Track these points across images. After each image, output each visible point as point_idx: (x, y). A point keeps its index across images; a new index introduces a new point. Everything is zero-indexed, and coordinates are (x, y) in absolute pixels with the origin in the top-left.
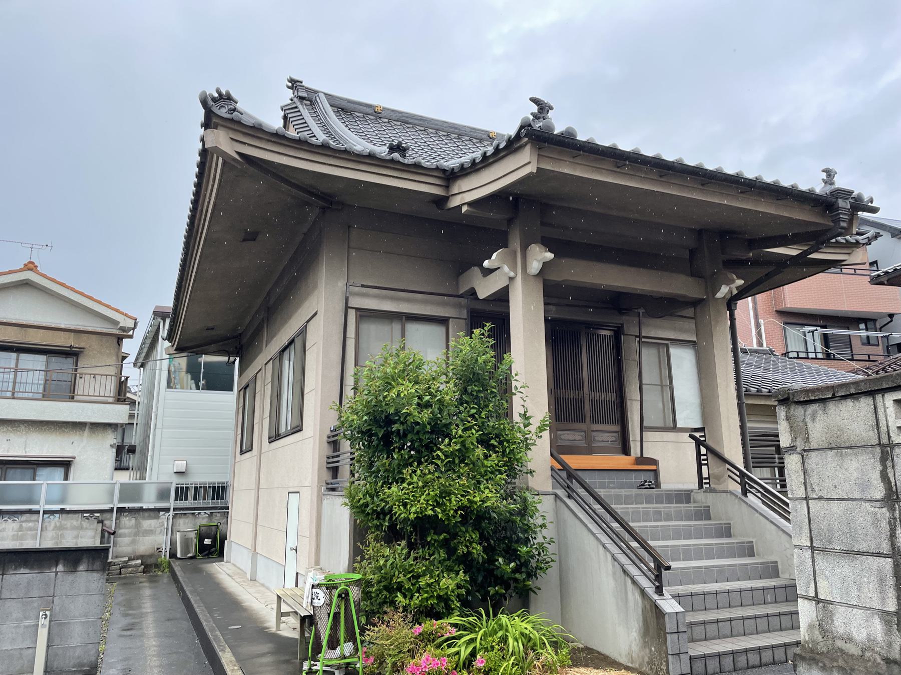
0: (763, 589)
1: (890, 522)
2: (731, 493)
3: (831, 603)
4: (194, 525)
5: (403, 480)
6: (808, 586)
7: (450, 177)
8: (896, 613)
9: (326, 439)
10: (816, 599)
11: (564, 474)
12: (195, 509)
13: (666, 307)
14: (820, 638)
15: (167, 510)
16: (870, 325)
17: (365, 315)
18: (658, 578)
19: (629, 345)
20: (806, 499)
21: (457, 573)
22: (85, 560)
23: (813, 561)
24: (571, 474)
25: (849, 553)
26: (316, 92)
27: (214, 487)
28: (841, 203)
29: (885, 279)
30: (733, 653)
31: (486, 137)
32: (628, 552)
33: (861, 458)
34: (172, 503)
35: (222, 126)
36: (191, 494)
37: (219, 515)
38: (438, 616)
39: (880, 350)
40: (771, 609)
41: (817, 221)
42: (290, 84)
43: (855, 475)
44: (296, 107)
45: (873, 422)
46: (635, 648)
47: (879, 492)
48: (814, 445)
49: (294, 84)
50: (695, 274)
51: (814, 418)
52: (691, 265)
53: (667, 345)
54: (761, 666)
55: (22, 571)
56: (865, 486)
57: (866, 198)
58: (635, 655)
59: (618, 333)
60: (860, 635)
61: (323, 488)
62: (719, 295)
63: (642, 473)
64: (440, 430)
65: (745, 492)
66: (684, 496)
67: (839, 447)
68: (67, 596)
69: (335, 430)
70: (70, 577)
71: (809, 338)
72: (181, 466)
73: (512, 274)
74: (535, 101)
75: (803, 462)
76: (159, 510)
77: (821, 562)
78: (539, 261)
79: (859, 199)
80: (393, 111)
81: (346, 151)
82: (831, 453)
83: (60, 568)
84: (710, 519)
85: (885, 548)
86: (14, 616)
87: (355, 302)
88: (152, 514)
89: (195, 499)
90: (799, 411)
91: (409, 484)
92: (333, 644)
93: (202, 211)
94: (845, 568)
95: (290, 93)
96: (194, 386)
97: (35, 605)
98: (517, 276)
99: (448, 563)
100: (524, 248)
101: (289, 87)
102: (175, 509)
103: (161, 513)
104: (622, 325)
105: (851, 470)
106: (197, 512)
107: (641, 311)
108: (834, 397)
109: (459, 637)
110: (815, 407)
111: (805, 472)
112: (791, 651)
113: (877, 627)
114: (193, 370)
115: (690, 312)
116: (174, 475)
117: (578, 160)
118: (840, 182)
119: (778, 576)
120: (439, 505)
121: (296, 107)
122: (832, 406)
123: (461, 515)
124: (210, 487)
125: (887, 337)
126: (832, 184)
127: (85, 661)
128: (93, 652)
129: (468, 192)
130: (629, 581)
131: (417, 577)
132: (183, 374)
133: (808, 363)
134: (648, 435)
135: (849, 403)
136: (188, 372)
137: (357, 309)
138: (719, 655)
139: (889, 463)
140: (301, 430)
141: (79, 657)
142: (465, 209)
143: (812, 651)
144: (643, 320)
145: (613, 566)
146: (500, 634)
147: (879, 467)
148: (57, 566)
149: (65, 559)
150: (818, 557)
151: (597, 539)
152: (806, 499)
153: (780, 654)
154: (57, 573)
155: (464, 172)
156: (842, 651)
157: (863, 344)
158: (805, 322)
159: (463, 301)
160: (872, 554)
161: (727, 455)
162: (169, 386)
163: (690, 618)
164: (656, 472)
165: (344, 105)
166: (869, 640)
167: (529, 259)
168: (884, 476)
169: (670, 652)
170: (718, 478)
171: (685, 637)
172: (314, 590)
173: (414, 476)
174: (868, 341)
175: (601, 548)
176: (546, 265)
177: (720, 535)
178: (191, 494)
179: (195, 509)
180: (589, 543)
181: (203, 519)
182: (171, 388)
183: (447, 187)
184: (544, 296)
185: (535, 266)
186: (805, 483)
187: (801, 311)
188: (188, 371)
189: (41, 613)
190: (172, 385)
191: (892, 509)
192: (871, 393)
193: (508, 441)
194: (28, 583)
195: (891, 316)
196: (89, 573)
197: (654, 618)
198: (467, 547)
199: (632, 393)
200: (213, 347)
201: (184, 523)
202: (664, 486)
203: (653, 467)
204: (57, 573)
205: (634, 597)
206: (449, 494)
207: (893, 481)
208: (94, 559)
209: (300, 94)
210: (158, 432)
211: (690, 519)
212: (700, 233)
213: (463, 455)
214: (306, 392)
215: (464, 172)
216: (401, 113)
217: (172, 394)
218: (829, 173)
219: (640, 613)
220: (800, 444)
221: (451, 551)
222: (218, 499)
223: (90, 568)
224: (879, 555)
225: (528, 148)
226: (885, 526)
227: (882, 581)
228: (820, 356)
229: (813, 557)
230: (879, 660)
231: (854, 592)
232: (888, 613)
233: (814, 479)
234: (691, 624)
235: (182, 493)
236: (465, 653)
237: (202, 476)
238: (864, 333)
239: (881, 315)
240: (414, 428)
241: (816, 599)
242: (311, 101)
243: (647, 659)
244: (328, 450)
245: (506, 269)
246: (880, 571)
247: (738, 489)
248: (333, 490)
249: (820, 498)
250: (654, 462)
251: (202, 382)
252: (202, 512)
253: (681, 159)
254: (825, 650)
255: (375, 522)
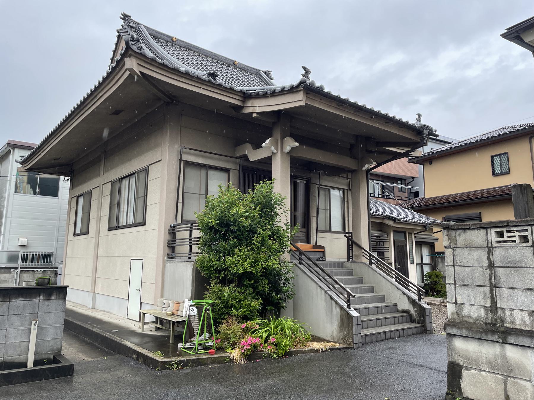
0: (382, 307)
1: (490, 275)
2: (364, 263)
3: (462, 304)
4: (34, 278)
5: (234, 254)
6: (452, 298)
7: (246, 96)
8: (490, 306)
9: (167, 231)
10: (456, 303)
11: (298, 253)
12: (34, 268)
13: (334, 171)
14: (457, 317)
15: (17, 268)
16: (403, 181)
17: (188, 164)
18: (349, 301)
19: (314, 189)
20: (454, 266)
21: (258, 299)
22: (55, 294)
23: (455, 289)
24: (301, 253)
25: (472, 286)
26: (139, 24)
27: (45, 255)
28: (425, 131)
29: (415, 161)
30: (376, 334)
31: (232, 63)
32: (334, 289)
33: (479, 251)
34: (20, 264)
35: (134, 56)
36: (30, 259)
37: (49, 272)
38: (251, 319)
39: (406, 195)
40: (384, 316)
41: (412, 138)
42: (122, 17)
43: (476, 257)
44: (127, 32)
45: (485, 238)
46: (336, 333)
47: (486, 263)
48: (459, 245)
49: (125, 17)
50: (353, 157)
51: (459, 235)
52: (350, 151)
53: (329, 190)
54: (385, 340)
55: (20, 299)
56: (480, 261)
57: (434, 129)
58: (335, 336)
59: (308, 182)
60: (474, 315)
61: (166, 257)
62: (364, 169)
63: (318, 253)
64: (252, 232)
65: (371, 263)
66: (340, 265)
67: (470, 247)
68: (45, 313)
69: (174, 227)
70: (47, 303)
71: (376, 186)
72: (23, 241)
73: (275, 151)
74: (304, 68)
75: (453, 252)
76: (11, 268)
77: (458, 289)
78: (290, 146)
79: (431, 130)
80: (183, 42)
81: (163, 65)
82: (466, 249)
83: (41, 298)
84: (352, 275)
85: (487, 283)
86: (16, 324)
87: (186, 157)
88: (6, 270)
89: (32, 262)
90: (453, 233)
91: (238, 256)
92: (202, 333)
93: (96, 96)
94: (470, 292)
95: (122, 22)
96: (32, 192)
97: (28, 318)
98: (277, 153)
99: (253, 295)
100: (283, 138)
101: (121, 18)
102: (21, 268)
103: (12, 270)
104: (311, 178)
105: (475, 255)
106: (36, 270)
107: (321, 172)
108: (470, 228)
109: (260, 329)
110: (461, 231)
111: (454, 255)
112: (397, 333)
113: (482, 312)
114: (32, 182)
115: (349, 175)
116: (19, 247)
117: (323, 101)
118: (423, 122)
119: (385, 302)
120: (252, 267)
121: (127, 32)
122: (468, 232)
123: (263, 272)
124: (36, 255)
125: (410, 188)
126: (420, 121)
127: (55, 348)
128: (59, 343)
129: (257, 107)
130: (334, 303)
131: (240, 301)
132: (25, 184)
133: (375, 199)
134: (319, 234)
135: (476, 231)
136: (28, 183)
137: (184, 161)
138: (371, 335)
139: (491, 254)
140: (145, 225)
141: (51, 346)
142: (254, 115)
143: (453, 322)
144: (321, 176)
145: (325, 296)
146: (280, 327)
147: (487, 255)
148: (39, 296)
149: (44, 293)
150: (457, 287)
151: (317, 284)
152: (454, 266)
153: (392, 335)
154: (39, 300)
155: (258, 96)
156: (466, 321)
157: (399, 191)
158: (374, 178)
159: (238, 161)
160: (482, 286)
161: (363, 246)
162: (16, 192)
163: (363, 319)
164: (324, 253)
165: (155, 33)
166: (478, 316)
167: (284, 145)
168: (489, 258)
169: (354, 333)
170: (358, 256)
171: (360, 327)
172: (191, 308)
173: (241, 252)
174: (401, 190)
175: (319, 288)
176: (293, 148)
177: (359, 283)
178: (30, 259)
179: (34, 268)
180: (312, 286)
181: (39, 274)
182: (18, 192)
183: (243, 102)
184: (291, 163)
185: (288, 149)
186: (453, 260)
187: (385, 175)
188: (28, 183)
189: (33, 323)
190: (18, 191)
191: (491, 270)
192: (486, 228)
193: (282, 237)
194: (24, 306)
195: (413, 178)
196: (57, 301)
197: (346, 320)
198: (263, 287)
199: (313, 213)
200: (49, 170)
201: (27, 276)
202: (327, 260)
203: (323, 250)
204: (39, 300)
205: (336, 311)
206: (258, 261)
207: (492, 260)
208: (59, 293)
209: (131, 25)
210: (9, 220)
211: (344, 275)
212: (357, 137)
213: (263, 243)
214: (148, 204)
215: (258, 96)
216: (187, 43)
217: (18, 197)
218: (419, 116)
219: (339, 316)
220: (452, 245)
221: (254, 289)
222: (47, 262)
223: (58, 298)
224: (484, 286)
225: (302, 93)
226: (487, 276)
227: (485, 296)
228: (380, 196)
229: (455, 288)
230: (482, 323)
231: (473, 300)
232: (487, 307)
233: (457, 259)
234: (362, 321)
235: (25, 258)
236: (265, 335)
237: (38, 247)
238: (400, 186)
239: (409, 177)
240: (241, 229)
241: (456, 303)
242: (136, 30)
243: (341, 337)
244: (168, 237)
245: (273, 148)
246: (484, 292)
247: (368, 263)
248: (172, 258)
249: (460, 266)
250: (323, 248)
251: (38, 190)
252: (39, 270)
253: (356, 102)
254: (459, 321)
255: (215, 275)
